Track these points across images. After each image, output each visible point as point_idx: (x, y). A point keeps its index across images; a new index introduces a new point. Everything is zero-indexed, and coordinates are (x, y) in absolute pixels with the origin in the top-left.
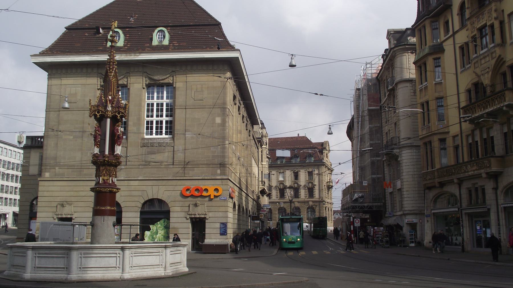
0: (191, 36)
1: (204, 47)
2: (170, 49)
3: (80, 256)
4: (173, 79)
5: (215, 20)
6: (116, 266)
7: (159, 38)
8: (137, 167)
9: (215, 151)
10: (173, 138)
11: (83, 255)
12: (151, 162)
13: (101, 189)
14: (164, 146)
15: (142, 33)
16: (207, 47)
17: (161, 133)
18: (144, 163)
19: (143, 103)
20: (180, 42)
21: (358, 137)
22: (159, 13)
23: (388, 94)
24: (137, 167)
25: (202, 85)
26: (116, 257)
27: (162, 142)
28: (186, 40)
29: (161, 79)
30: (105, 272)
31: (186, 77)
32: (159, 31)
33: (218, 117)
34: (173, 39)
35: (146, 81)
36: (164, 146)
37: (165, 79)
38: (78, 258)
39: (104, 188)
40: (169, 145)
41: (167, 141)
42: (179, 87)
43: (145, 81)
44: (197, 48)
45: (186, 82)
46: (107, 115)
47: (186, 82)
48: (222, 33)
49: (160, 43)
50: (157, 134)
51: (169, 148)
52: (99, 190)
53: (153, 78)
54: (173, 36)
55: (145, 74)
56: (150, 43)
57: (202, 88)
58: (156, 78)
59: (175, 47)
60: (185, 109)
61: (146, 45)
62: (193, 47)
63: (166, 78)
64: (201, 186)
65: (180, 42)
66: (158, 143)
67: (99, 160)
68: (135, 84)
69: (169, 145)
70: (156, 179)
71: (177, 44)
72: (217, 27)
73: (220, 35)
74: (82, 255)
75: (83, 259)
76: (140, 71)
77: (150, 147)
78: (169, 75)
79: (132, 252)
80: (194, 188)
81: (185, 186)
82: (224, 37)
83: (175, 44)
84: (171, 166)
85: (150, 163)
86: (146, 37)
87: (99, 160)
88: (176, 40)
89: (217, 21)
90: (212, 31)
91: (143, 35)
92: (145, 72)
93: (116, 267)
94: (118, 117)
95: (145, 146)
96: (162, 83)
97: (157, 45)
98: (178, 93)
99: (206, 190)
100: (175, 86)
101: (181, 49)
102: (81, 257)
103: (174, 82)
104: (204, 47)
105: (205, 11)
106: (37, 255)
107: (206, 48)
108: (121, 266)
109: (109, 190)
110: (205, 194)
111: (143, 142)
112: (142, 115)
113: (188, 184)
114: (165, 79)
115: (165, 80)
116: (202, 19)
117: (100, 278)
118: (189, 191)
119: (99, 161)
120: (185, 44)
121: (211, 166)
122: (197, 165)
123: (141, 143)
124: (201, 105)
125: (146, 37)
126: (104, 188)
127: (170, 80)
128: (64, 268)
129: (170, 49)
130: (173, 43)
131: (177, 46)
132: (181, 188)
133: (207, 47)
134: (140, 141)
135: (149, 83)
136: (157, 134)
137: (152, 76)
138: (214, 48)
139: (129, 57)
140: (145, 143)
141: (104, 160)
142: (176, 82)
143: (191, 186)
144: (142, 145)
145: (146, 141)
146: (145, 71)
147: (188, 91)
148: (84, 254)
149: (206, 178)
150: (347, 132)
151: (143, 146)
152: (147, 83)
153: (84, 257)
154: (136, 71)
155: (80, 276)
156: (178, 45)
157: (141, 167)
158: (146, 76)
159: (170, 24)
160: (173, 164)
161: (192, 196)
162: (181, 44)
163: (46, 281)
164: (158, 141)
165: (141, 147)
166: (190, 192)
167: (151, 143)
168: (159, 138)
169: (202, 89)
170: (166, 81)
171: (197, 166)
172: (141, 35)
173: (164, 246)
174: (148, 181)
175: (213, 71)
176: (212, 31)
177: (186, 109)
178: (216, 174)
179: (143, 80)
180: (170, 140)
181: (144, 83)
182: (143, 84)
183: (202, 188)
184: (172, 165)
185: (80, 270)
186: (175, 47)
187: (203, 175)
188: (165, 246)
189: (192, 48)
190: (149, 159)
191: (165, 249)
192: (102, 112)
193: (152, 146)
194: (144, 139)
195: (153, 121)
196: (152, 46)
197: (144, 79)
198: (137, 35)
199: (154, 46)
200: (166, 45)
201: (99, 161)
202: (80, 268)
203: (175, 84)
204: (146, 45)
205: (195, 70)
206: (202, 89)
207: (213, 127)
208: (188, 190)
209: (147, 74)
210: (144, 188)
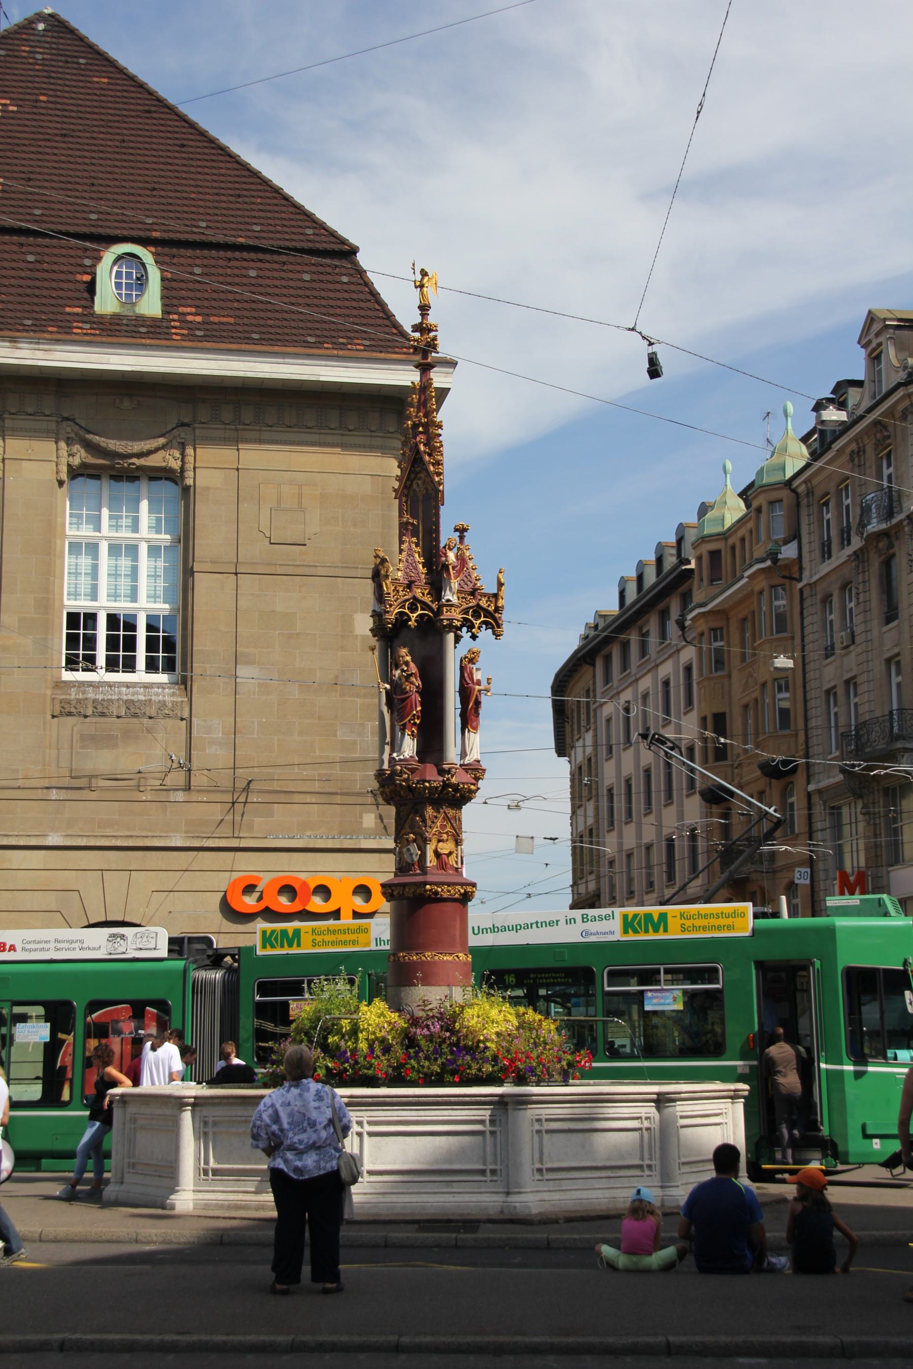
0: (269, 290)
1: (310, 339)
2: (176, 334)
3: (537, 1127)
4: (183, 455)
5: (332, 234)
6: (641, 1163)
7: (118, 286)
8: (39, 794)
9: (354, 743)
10: (185, 683)
11: (365, 1125)
12: (96, 776)
13: (439, 890)
14: (151, 718)
15: (39, 258)
16: (321, 340)
17: (130, 665)
18: (66, 782)
19: (58, 542)
20: (207, 311)
21: (637, 700)
22: (95, 182)
23: (849, 551)
24: (39, 794)
25: (300, 486)
26: (640, 1129)
27: (143, 698)
28: (230, 305)
29: (135, 451)
30: (612, 1183)
31: (238, 450)
32: (119, 259)
33: (362, 612)
34: (174, 293)
35: (71, 455)
36: (151, 718)
37: (150, 453)
38: (533, 1136)
39: (449, 884)
40: (171, 713)
41: (161, 698)
42: (207, 489)
43: (66, 454)
44: (285, 343)
45: (238, 469)
46: (448, 620)
47: (238, 469)
48: (367, 289)
49: (129, 306)
50: (112, 664)
51: (169, 722)
52: (431, 890)
53: (103, 444)
54: (174, 284)
55: (68, 428)
56: (83, 303)
57: (300, 495)
58: (114, 445)
59: (191, 329)
60: (234, 576)
61: (68, 310)
62: (265, 336)
63: (157, 450)
64: (302, 876)
65: (207, 311)
66: (127, 701)
67: (429, 782)
68: (25, 464)
69: (171, 713)
70: (119, 843)
71: (199, 319)
72: (344, 263)
73: (362, 296)
74: (362, 1127)
75: (546, 1137)
76: (48, 412)
77: (94, 720)
78: (162, 441)
79: (648, 1115)
80: (274, 881)
81: (236, 875)
82: (377, 307)
83: (190, 318)
84: (180, 796)
85: (94, 781)
86: (62, 276)
87: (429, 782)
88: (189, 302)
89: (343, 241)
90: (329, 278)
91: (46, 266)
92: (67, 419)
93: (640, 1167)
94: (410, 620)
95: (70, 714)
96: (140, 468)
97: (115, 316)
98: (203, 511)
99: (324, 891)
100: (189, 482)
101: (220, 339)
102: (538, 1132)
103: (187, 466)
104: (310, 339)
105: (280, 194)
106: (367, 1128)
107: (319, 345)
108: (656, 1163)
109: (462, 891)
110: (317, 904)
111: (62, 697)
112: (57, 590)
113: (248, 864)
114: (150, 453)
115: (152, 457)
116: (276, 225)
117: (604, 1207)
118: (256, 895)
119: (427, 784)
120: (232, 320)
121: (338, 799)
122: (285, 796)
123: (53, 699)
124: (298, 563)
125: (62, 276)
126: (449, 884)
127: (170, 459)
128: (482, 1172)
129: (176, 334)
130: (181, 309)
131: (199, 326)
132: (223, 882)
133: (321, 340)
134: (49, 692)
135: (84, 465)
136: (112, 664)
137: (97, 438)
138: (349, 347)
139: (40, 354)
140: (74, 703)
141: (443, 781)
142: (195, 468)
143: (261, 875)
144: (58, 708)
145: (73, 695)
146: (66, 415)
147: (243, 506)
148: (370, 1123)
149: (320, 844)
150: (557, 676)
151: (61, 714)
152: (76, 461)
153: (371, 1134)
154: (30, 410)
155: (546, 1198)
156: (204, 323)
157: (54, 794)
158: (72, 435)
159: (156, 234)
160: (188, 788)
161: (269, 914)
162: (215, 319)
163: (452, 1217)
164: (125, 692)
165: (53, 717)
166: (260, 899)
167: (94, 701)
168: (82, 684)
169: (300, 503)
170: (155, 461)
171: (282, 797)
172: (38, 266)
173: (655, 1096)
174: (164, 853)
175: (342, 435)
176: (329, 278)
177: (236, 574)
178: (358, 830)
179: (57, 449)
180: (173, 695)
181: (64, 461)
182: (60, 467)
183: (305, 884)
184: (184, 790)
185: (541, 1178)
186: (191, 329)
187: (308, 833)
188: (735, 1091)
189: (261, 339)
190: (88, 767)
191: (732, 1103)
192: (425, 606)
193: (103, 715)
194: (60, 685)
195: (136, 615)
196: (93, 314)
197: (63, 445)
198: (22, 265)
199: (102, 316)
200: (153, 319)
201: (427, 784)
202: (540, 1170)
203: (191, 474)
204: (68, 310)
205: (271, 426)
206: (300, 503)
207: (343, 648)
208: (249, 889)
209: (76, 428)
210: (68, 879)
